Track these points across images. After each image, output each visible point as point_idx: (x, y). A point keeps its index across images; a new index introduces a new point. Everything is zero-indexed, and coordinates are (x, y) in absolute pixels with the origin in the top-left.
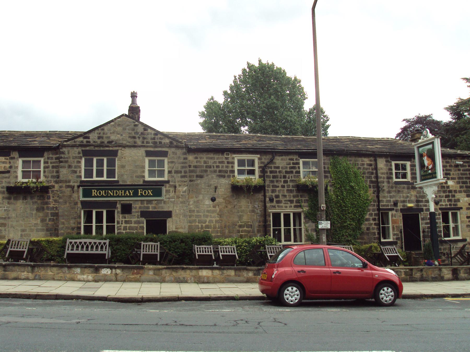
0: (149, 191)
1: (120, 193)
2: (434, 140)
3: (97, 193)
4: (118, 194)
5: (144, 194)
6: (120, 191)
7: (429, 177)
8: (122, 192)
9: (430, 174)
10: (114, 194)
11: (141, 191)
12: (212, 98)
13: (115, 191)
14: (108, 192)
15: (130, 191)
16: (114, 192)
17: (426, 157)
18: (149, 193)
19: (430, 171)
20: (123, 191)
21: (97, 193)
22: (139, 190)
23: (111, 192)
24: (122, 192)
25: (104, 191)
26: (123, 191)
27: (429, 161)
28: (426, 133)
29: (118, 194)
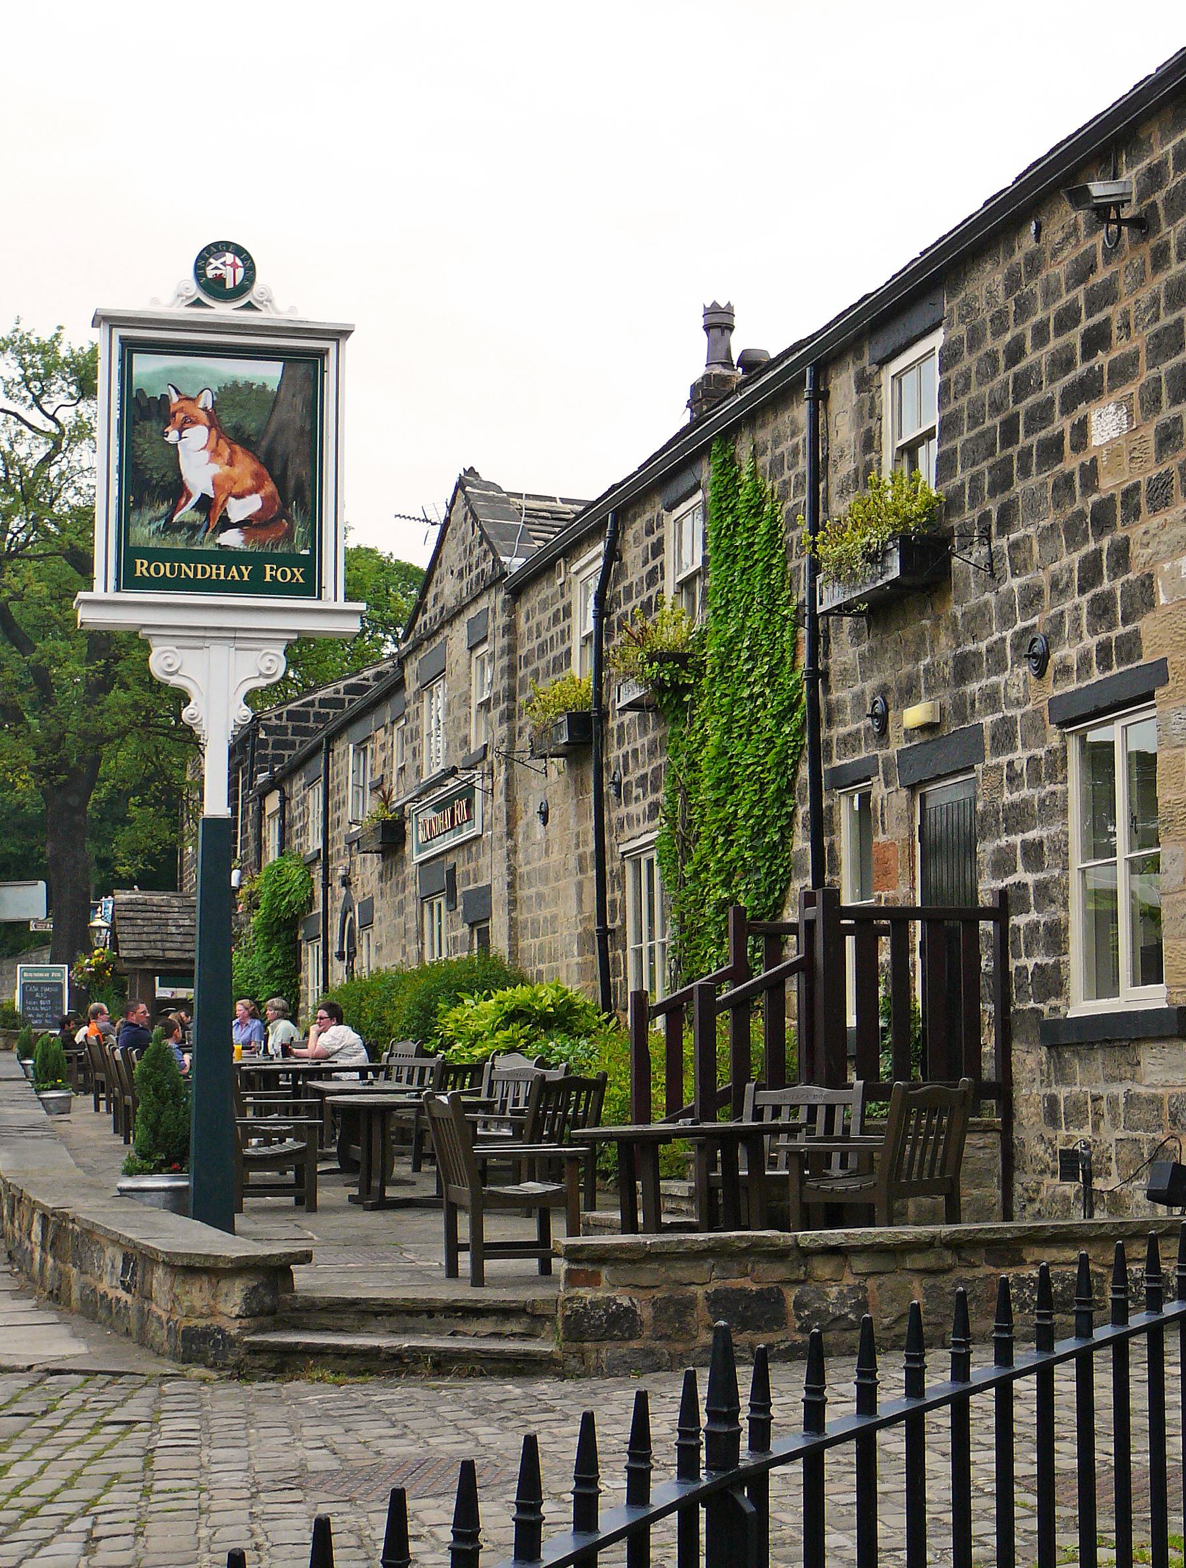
0: (295, 570)
1: (214, 571)
2: (331, 346)
3: (148, 569)
4: (208, 575)
5: (280, 579)
6: (214, 567)
7: (214, 571)
8: (218, 569)
9: (226, 556)
10: (195, 574)
11: (272, 569)
12: (340, 335)
13: (199, 566)
14: (180, 567)
15: (243, 568)
16: (195, 568)
17: (198, 436)
18: (293, 575)
19: (232, 539)
20: (222, 567)
21: (148, 569)
22: (268, 567)
23: (190, 568)
24: (218, 569)
25: (168, 565)
26: (222, 567)
27: (231, 463)
28: (240, 273)
29: (208, 575)
